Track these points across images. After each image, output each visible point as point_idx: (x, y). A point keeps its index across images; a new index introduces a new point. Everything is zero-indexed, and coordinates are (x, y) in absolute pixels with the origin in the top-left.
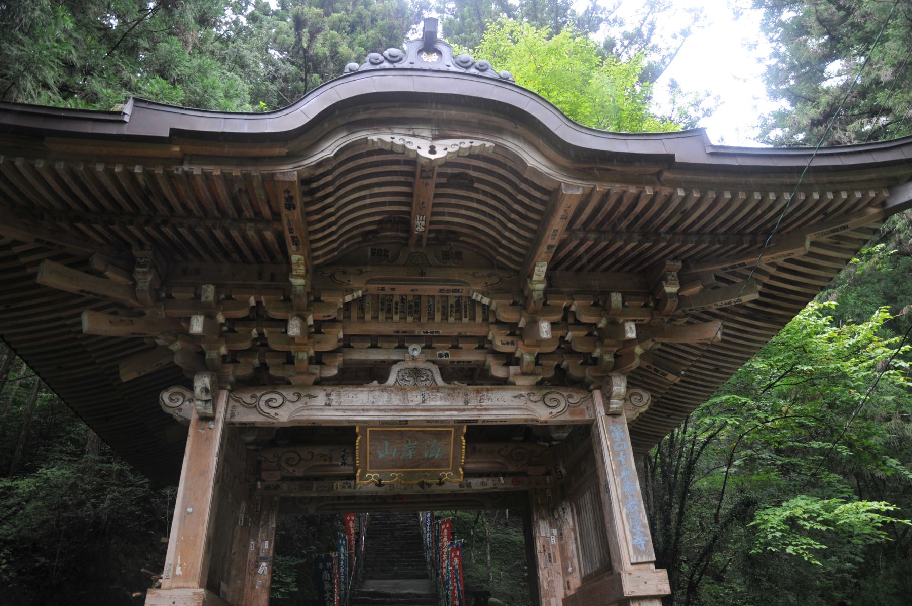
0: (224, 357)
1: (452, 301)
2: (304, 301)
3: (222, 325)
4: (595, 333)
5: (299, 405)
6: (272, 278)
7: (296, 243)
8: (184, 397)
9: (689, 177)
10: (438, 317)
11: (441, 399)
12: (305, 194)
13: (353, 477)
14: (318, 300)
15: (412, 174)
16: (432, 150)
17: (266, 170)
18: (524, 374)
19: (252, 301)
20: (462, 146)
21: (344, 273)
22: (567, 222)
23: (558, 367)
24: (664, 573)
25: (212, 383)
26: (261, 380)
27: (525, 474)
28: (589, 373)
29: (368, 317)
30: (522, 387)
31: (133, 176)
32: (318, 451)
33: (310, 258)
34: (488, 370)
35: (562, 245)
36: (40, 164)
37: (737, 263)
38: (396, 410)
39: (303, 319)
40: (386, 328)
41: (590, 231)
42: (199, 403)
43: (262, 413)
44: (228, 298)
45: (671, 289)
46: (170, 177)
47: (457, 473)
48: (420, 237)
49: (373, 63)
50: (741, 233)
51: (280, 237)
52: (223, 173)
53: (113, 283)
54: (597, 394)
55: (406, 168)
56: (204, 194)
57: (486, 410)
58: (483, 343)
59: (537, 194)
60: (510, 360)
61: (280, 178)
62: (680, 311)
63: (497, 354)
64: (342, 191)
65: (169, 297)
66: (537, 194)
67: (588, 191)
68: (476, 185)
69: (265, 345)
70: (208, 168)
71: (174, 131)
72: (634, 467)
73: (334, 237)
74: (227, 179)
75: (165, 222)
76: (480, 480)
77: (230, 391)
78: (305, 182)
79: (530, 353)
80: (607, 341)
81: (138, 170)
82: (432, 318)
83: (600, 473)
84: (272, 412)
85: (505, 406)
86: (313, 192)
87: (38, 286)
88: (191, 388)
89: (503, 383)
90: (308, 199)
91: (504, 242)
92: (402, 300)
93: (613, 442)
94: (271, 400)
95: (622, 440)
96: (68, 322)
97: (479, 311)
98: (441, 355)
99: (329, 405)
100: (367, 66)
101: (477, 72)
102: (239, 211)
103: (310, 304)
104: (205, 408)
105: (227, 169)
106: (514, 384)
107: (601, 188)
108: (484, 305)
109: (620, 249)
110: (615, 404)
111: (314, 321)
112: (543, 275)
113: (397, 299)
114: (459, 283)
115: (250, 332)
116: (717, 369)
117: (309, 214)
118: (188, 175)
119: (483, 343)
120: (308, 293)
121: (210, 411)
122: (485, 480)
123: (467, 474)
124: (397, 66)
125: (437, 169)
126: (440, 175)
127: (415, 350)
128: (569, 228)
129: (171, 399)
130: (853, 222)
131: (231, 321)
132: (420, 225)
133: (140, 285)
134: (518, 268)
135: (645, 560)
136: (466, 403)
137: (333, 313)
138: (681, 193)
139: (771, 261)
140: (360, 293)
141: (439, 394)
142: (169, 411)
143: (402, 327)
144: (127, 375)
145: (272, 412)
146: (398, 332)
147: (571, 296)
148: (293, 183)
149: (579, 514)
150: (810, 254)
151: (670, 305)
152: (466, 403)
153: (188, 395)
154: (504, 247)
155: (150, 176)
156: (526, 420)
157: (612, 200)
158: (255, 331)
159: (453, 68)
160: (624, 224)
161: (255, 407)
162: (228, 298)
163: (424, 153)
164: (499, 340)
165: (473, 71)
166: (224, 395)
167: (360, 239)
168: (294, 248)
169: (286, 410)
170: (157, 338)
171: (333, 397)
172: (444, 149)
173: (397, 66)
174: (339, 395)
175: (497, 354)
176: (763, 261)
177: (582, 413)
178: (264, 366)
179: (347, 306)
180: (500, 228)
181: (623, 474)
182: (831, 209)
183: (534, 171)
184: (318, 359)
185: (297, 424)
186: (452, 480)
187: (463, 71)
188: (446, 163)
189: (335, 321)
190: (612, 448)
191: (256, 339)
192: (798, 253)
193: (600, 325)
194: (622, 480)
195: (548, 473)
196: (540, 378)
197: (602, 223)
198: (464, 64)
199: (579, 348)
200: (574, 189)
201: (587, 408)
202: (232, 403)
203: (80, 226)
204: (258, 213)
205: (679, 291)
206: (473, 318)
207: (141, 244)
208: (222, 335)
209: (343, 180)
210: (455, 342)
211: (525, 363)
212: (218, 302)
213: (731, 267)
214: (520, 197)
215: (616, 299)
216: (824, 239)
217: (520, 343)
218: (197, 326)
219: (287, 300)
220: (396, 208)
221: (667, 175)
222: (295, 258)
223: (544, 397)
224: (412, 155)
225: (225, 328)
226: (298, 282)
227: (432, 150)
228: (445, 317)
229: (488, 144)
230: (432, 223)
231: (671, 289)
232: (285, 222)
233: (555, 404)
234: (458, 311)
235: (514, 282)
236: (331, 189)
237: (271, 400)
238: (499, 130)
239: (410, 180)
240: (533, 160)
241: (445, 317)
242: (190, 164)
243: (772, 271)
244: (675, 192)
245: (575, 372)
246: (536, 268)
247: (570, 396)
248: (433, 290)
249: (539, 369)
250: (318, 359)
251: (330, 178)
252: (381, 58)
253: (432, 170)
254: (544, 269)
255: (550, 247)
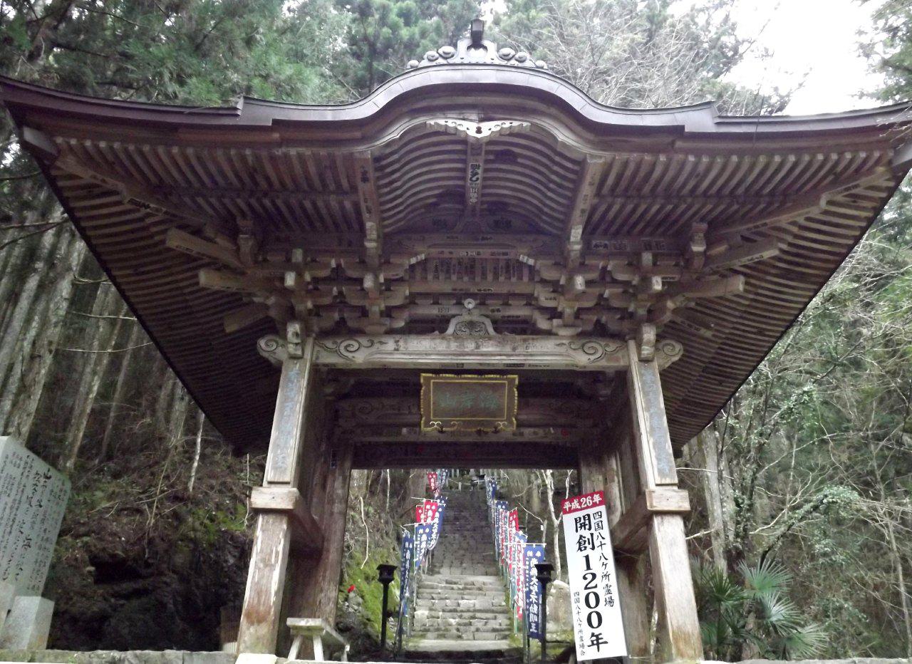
0: (310, 311)
1: (502, 264)
2: (376, 261)
3: (309, 283)
4: (631, 291)
5: (374, 349)
6: (350, 244)
7: (369, 211)
8: (277, 343)
9: (711, 145)
10: (490, 277)
11: (492, 345)
12: (377, 170)
13: (418, 425)
14: (388, 262)
15: (465, 152)
16: (479, 131)
17: (345, 150)
18: (565, 326)
19: (333, 263)
20: (504, 126)
21: (410, 239)
22: (594, 188)
23: (598, 321)
24: (685, 493)
25: (301, 329)
26: (341, 330)
27: (573, 426)
28: (626, 326)
29: (430, 277)
30: (563, 337)
31: (243, 159)
32: (386, 402)
33: (381, 226)
34: (534, 324)
35: (594, 209)
36: (175, 150)
37: (759, 223)
38: (454, 355)
39: (376, 277)
40: (447, 288)
41: (617, 196)
42: (291, 345)
43: (341, 355)
44: (314, 261)
45: (698, 248)
46: (273, 159)
47: (511, 423)
48: (474, 209)
49: (430, 60)
50: (758, 194)
51: (356, 206)
52: (298, 154)
53: (221, 247)
54: (632, 344)
55: (459, 147)
56: (298, 169)
57: (531, 355)
58: (530, 300)
59: (569, 165)
60: (553, 314)
61: (357, 155)
62: (707, 270)
63: (543, 310)
64: (407, 168)
65: (265, 260)
66: (569, 165)
67: (609, 160)
68: (520, 160)
69: (344, 303)
70: (301, 150)
71: (276, 122)
72: (662, 406)
73: (401, 208)
74: (317, 159)
75: (266, 195)
76: (532, 430)
77: (315, 339)
78: (377, 159)
79: (572, 307)
80: (640, 297)
81: (248, 152)
82: (484, 275)
83: (634, 418)
84: (350, 355)
85: (549, 353)
86: (382, 168)
87: (169, 250)
88: (284, 337)
89: (549, 333)
90: (378, 174)
91: (546, 210)
92: (460, 263)
93: (644, 383)
94: (349, 345)
95: (653, 382)
96: (181, 284)
97: (526, 272)
98: (493, 311)
99: (397, 350)
100: (425, 63)
101: (516, 63)
102: (324, 185)
103: (381, 265)
104: (296, 350)
105: (315, 150)
106: (556, 334)
107: (621, 157)
108: (530, 266)
109: (646, 211)
110: (647, 351)
111: (385, 280)
112: (579, 237)
113: (454, 262)
114: (508, 246)
115: (332, 290)
116: (761, 332)
117: (379, 187)
118: (286, 156)
119: (530, 300)
120: (380, 256)
121: (299, 353)
122: (536, 430)
123: (520, 425)
124: (451, 61)
125: (484, 148)
126: (488, 152)
127: (470, 304)
128: (598, 194)
129: (267, 345)
130: (864, 181)
131: (316, 280)
132: (473, 197)
133: (243, 250)
134: (559, 233)
135: (668, 481)
136: (514, 349)
137: (401, 274)
138: (691, 158)
139: (790, 220)
140: (423, 257)
141: (491, 342)
142: (265, 355)
143: (460, 285)
144: (231, 327)
145: (350, 355)
146: (455, 290)
147: (607, 256)
148: (366, 160)
149: (621, 460)
150: (826, 213)
151: (698, 263)
152: (514, 349)
153: (281, 342)
154: (546, 214)
155: (258, 158)
156: (567, 365)
157: (632, 167)
158: (335, 289)
159: (497, 61)
160: (647, 189)
161: (337, 352)
162: (314, 261)
163: (472, 133)
164: (544, 297)
165: (513, 62)
166: (310, 341)
167: (423, 210)
168: (367, 215)
169: (360, 354)
170: (255, 295)
171: (401, 343)
172: (490, 128)
173: (451, 61)
174: (406, 342)
175: (543, 310)
176: (783, 220)
177: (617, 360)
178: (342, 321)
179: (412, 267)
180: (542, 198)
181: (652, 411)
182: (839, 169)
183: (564, 144)
184: (388, 313)
185: (370, 367)
186: (506, 428)
187: (504, 63)
188: (491, 142)
189: (401, 280)
190: (643, 389)
191: (335, 297)
192: (814, 212)
193: (634, 282)
194: (651, 415)
195: (596, 425)
196: (580, 330)
197: (626, 190)
198: (506, 57)
199: (616, 303)
200: (597, 159)
201: (623, 356)
202: (317, 348)
203: (200, 200)
204: (339, 185)
205: (705, 251)
206: (520, 278)
207: (244, 215)
208: (308, 292)
209: (407, 159)
210: (506, 299)
211: (566, 316)
212: (306, 264)
213: (755, 227)
214: (555, 168)
215: (647, 258)
216: (839, 198)
217: (562, 298)
218: (290, 280)
219: (362, 262)
220: (451, 183)
221: (679, 144)
222: (369, 225)
223: (583, 346)
224: (463, 135)
225: (311, 287)
226: (370, 245)
227: (479, 131)
228: (496, 276)
229: (525, 124)
230: (483, 195)
231: (698, 248)
232: (361, 194)
233: (592, 352)
234: (508, 271)
235: (554, 246)
236: (396, 166)
237: (349, 345)
238: (534, 112)
239: (464, 157)
240: (563, 135)
241: (496, 276)
242: (288, 146)
243: (795, 230)
244: (658, 158)
245: (613, 326)
246: (573, 231)
247: (607, 345)
248: (486, 253)
249: (579, 322)
250: (388, 313)
251: (396, 156)
252: (437, 55)
253: (480, 148)
254: (580, 231)
255: (583, 211)
